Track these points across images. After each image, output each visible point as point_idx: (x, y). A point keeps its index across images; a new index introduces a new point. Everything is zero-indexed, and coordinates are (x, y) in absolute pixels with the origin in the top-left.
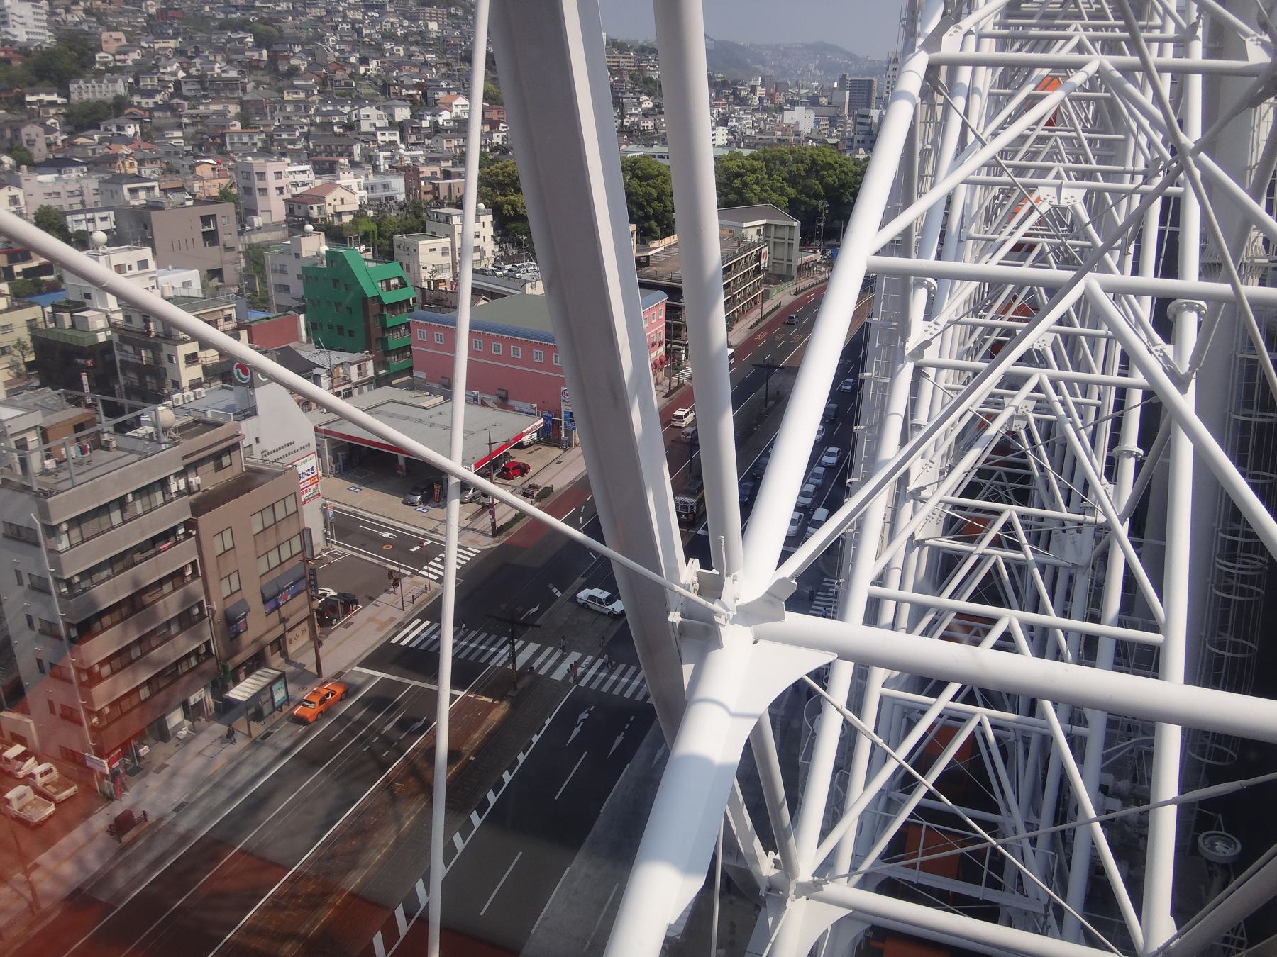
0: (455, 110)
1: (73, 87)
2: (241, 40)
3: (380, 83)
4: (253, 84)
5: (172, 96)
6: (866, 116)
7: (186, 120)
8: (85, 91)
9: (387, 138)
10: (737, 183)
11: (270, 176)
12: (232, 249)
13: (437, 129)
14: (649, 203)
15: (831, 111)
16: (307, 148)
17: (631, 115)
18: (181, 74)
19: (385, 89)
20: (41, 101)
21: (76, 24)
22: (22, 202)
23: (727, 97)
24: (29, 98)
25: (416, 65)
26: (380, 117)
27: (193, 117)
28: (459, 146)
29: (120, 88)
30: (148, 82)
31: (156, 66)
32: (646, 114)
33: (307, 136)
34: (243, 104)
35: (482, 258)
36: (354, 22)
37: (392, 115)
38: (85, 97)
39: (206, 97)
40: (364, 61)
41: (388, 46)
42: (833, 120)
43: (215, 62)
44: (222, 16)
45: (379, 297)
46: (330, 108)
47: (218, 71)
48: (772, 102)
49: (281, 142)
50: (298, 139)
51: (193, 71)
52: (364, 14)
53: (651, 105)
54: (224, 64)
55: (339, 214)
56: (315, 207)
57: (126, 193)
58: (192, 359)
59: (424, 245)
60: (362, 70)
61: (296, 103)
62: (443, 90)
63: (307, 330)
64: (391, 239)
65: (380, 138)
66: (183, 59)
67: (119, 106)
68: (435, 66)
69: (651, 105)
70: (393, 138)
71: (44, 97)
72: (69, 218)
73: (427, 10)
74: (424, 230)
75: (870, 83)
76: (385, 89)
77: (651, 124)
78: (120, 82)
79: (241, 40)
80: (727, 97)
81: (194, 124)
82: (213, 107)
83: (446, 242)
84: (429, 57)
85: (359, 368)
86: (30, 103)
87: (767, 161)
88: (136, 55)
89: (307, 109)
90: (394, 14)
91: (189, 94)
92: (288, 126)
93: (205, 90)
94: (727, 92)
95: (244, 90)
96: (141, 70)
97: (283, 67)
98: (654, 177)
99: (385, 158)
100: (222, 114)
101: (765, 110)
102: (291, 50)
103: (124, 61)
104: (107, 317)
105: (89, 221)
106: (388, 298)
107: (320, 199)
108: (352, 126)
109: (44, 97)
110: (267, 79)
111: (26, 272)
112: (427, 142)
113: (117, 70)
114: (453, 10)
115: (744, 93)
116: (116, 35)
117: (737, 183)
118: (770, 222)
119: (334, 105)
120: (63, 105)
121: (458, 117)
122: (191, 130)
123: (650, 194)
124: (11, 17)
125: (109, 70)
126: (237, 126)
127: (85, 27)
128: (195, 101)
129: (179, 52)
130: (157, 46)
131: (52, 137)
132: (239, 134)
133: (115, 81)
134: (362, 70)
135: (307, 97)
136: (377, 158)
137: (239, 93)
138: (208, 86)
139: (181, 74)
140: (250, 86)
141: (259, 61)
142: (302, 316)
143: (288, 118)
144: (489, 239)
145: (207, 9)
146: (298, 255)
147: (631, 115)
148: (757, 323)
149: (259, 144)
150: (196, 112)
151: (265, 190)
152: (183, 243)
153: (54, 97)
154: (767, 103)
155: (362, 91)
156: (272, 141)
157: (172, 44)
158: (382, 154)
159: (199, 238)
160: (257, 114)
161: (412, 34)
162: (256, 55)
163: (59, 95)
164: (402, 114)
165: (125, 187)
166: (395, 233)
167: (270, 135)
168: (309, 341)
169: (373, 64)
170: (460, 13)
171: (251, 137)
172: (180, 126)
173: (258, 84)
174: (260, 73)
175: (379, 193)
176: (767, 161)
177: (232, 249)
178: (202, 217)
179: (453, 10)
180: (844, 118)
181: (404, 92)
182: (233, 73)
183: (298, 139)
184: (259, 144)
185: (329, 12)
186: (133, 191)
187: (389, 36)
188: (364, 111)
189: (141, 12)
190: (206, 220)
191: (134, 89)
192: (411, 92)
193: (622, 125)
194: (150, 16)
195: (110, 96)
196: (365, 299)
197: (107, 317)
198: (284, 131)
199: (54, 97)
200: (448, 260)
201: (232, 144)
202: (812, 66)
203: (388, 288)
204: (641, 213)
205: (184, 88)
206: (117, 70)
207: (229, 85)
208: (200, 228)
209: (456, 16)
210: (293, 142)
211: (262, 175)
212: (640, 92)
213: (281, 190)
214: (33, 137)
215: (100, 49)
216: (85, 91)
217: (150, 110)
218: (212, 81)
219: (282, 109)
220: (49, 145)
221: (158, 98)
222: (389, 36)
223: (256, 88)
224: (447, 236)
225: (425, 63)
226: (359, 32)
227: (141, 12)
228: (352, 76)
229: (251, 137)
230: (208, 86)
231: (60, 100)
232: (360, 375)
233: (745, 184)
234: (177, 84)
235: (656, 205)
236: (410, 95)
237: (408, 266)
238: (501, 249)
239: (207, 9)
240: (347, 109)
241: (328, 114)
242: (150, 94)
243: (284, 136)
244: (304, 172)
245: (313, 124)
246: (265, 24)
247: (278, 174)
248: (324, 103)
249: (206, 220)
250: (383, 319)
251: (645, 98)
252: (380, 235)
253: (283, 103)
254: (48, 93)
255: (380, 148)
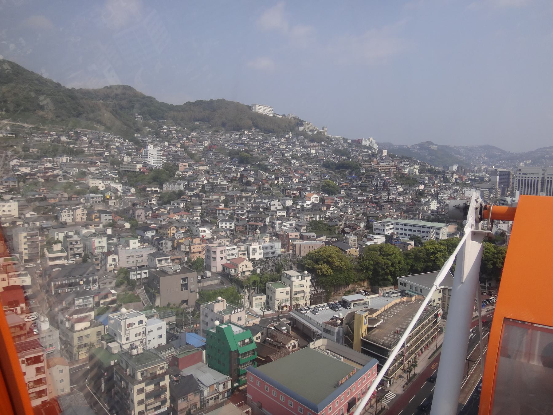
0: (312, 200)
1: (164, 186)
2: (231, 168)
3: (282, 188)
4: (232, 187)
5: (200, 191)
6: (505, 201)
7: (203, 202)
8: (168, 187)
9: (281, 214)
10: (432, 257)
11: (218, 253)
12: (194, 291)
13: (303, 209)
14: (387, 267)
15: (490, 186)
16: (248, 217)
17: (393, 194)
18: (206, 182)
19: (284, 191)
20: (152, 190)
21: (176, 152)
22: (117, 260)
23: (440, 179)
24: (147, 189)
25: (303, 170)
26: (279, 205)
27: (206, 201)
28: (311, 218)
29: (182, 187)
30: (192, 185)
31: (197, 178)
32: (399, 194)
33: (249, 212)
34: (226, 196)
35: (304, 296)
36: (281, 150)
37: (285, 203)
38: (169, 189)
39: (213, 192)
40: (277, 178)
41: (293, 162)
42: (491, 190)
43: (219, 177)
44: (231, 148)
45: (237, 350)
46: (259, 200)
47: (219, 181)
48: (462, 180)
49: (238, 215)
50: (245, 213)
51: (210, 180)
52: (287, 146)
53: (402, 190)
54: (223, 178)
55: (244, 272)
56: (233, 270)
57: (157, 262)
58: (141, 391)
59: (278, 291)
60: (276, 182)
61: (246, 197)
62: (308, 191)
63: (206, 357)
64: (265, 284)
65: (278, 214)
66: (207, 175)
67: (179, 195)
68: (311, 170)
69: (402, 190)
70: (283, 214)
71: (153, 189)
72: (131, 273)
73: (312, 144)
74: (281, 280)
75: (509, 173)
76: (284, 191)
77: (401, 198)
78: (182, 185)
79: (231, 168)
80: (440, 179)
81: (206, 204)
82: (215, 197)
83: (288, 289)
84: (309, 166)
85: (224, 385)
86: (148, 191)
87: (448, 245)
88: (190, 173)
89: (250, 200)
90: (299, 146)
91: (207, 190)
92: (242, 207)
93: (213, 189)
94: (440, 176)
95: (228, 190)
96: (193, 179)
97: (245, 180)
98: (390, 255)
99: (279, 224)
100: (218, 200)
101: (458, 184)
102: (249, 173)
103: (186, 175)
104: (121, 347)
105: (138, 274)
106: (241, 351)
107: (236, 266)
108: (267, 208)
109: (153, 189)
110: (238, 185)
111: (104, 303)
112: (298, 215)
113: (183, 178)
114: (323, 143)
115: (448, 177)
116: (185, 164)
117: (432, 257)
118: (446, 287)
119: (261, 199)
120: (160, 193)
121: (313, 202)
122: (204, 206)
123: (388, 264)
124: (149, 155)
125: (179, 178)
126: (222, 206)
127: (179, 153)
128: (208, 193)
129: (207, 172)
130: (200, 168)
131: (148, 213)
132: (222, 211)
133: (180, 184)
134: (276, 182)
135: (252, 194)
136: (275, 224)
137: (226, 191)
138: (215, 188)
139: (206, 182)
140: (231, 189)
141: (236, 177)
142: (204, 351)
143: (242, 204)
144: (308, 287)
145: (226, 145)
146: (213, 311)
147: (393, 194)
148: (433, 354)
149: (230, 214)
150: (208, 198)
151: (215, 258)
152: (172, 290)
153: (157, 189)
154: (459, 181)
155: (274, 192)
156: (234, 213)
157: (205, 168)
158: (277, 222)
159: (180, 287)
160: (231, 200)
161: (304, 155)
162: (235, 175)
163: (159, 188)
164: (289, 203)
165: (157, 259)
166: (267, 282)
167: (234, 210)
168: (206, 364)
169: (281, 179)
170: (326, 144)
171: (227, 211)
172: (200, 204)
173: (234, 187)
174: (236, 182)
175: (269, 250)
176: (448, 245)
177: (194, 291)
178: (182, 279)
179: (323, 143)
180: (496, 189)
181: (292, 192)
182: (225, 183)
183: (245, 213)
184: (230, 214)
185: (273, 146)
186: (160, 261)
187: (294, 157)
188: (272, 203)
189: (202, 145)
190: (184, 279)
191: (187, 187)
192: (295, 192)
193: (388, 199)
194: (205, 147)
195: (178, 189)
196: (230, 352)
197: (121, 347)
198: (240, 210)
199: (157, 189)
200: (289, 296)
201: (219, 214)
202: (483, 155)
203: (244, 344)
204: (383, 272)
205: (206, 187)
206: (183, 178)
207: (223, 187)
208: (181, 282)
209: (323, 145)
210: (243, 215)
211: (215, 252)
212: (398, 184)
213: (222, 258)
214: (140, 214)
215: (178, 169)
216: (168, 187)
217: (191, 196)
218: (216, 186)
219: (241, 200)
220: (146, 217)
221: (195, 192)
222: (294, 157)
223: (233, 189)
224: (289, 286)
225: (307, 169)
226: (283, 154)
227: (202, 145)
228: (271, 185)
229: (227, 211)
230: (215, 188)
231: (159, 190)
232: (223, 388)
233: (436, 258)
234: (203, 186)
235: (391, 268)
236: (294, 194)
237: (271, 298)
238: (315, 290)
239: (226, 145)
240: (266, 201)
241: (259, 203)
242: (192, 190)
243: (240, 212)
244: (234, 249)
245: (252, 206)
246: (246, 152)
247: (222, 252)
248: (258, 198)
249: (184, 279)
250: (238, 359)
251: (400, 187)
252: (261, 282)
253: (241, 197)
254: (155, 188)
255: (278, 219)
